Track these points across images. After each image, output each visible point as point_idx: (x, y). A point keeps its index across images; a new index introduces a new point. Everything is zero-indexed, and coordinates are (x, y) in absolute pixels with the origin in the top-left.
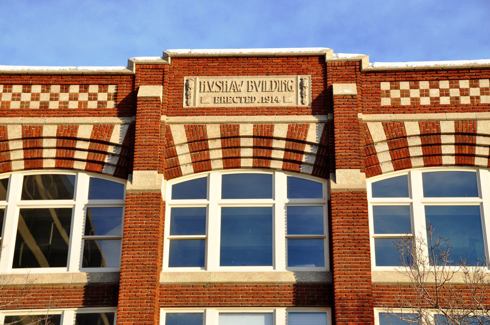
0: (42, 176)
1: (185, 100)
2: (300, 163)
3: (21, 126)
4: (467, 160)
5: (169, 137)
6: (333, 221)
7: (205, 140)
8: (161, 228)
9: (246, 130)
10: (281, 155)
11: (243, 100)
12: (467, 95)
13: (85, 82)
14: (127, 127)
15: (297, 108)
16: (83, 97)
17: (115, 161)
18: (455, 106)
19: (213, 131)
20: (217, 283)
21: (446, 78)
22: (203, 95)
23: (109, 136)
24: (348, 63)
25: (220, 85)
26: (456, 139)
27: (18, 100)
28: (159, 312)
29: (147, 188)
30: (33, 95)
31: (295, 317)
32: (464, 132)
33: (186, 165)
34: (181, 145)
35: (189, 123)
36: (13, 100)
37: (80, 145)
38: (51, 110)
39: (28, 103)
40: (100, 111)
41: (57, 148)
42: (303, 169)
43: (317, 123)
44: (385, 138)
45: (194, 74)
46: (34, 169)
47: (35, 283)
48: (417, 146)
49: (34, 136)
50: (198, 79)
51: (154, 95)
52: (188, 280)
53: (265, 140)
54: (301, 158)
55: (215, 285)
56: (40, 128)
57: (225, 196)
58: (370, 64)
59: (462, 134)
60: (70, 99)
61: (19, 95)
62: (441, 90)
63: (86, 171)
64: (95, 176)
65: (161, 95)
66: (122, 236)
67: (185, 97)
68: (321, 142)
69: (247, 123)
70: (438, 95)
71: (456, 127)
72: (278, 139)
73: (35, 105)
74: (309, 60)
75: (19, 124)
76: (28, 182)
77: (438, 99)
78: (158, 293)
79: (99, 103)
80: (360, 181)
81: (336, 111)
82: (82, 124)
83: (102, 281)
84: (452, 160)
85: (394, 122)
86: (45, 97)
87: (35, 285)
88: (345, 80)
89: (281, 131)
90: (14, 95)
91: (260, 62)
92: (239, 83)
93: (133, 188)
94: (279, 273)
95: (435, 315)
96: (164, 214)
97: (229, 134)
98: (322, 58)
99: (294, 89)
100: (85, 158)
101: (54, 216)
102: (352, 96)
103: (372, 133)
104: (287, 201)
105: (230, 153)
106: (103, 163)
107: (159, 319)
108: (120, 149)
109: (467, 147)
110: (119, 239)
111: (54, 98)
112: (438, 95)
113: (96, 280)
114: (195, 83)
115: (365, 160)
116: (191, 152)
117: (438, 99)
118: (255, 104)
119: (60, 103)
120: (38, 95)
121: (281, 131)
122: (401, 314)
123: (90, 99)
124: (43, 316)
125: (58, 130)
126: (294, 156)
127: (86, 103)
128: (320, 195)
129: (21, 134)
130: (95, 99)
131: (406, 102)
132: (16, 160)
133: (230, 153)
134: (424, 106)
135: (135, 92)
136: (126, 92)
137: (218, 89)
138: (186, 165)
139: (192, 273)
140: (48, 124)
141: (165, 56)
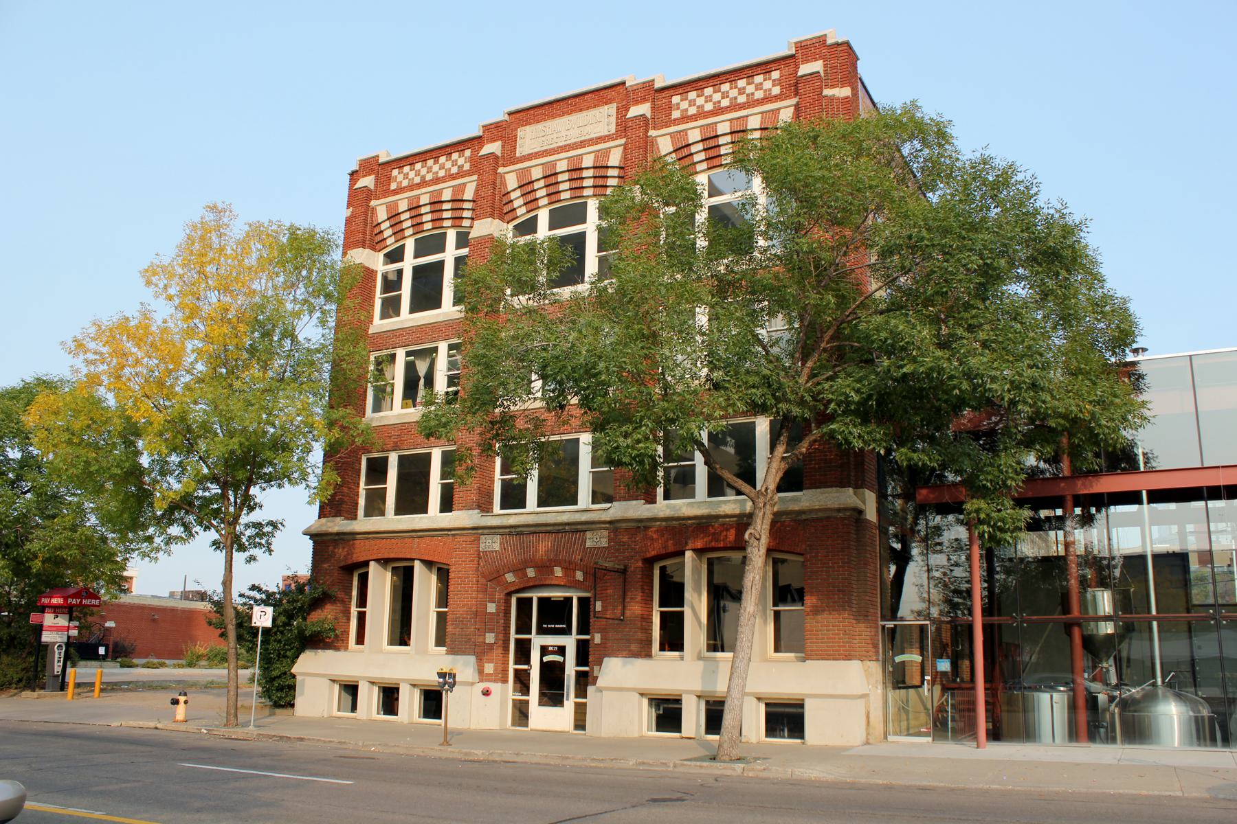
30: (690, 101)
63: (453, 226)
100: (449, 216)
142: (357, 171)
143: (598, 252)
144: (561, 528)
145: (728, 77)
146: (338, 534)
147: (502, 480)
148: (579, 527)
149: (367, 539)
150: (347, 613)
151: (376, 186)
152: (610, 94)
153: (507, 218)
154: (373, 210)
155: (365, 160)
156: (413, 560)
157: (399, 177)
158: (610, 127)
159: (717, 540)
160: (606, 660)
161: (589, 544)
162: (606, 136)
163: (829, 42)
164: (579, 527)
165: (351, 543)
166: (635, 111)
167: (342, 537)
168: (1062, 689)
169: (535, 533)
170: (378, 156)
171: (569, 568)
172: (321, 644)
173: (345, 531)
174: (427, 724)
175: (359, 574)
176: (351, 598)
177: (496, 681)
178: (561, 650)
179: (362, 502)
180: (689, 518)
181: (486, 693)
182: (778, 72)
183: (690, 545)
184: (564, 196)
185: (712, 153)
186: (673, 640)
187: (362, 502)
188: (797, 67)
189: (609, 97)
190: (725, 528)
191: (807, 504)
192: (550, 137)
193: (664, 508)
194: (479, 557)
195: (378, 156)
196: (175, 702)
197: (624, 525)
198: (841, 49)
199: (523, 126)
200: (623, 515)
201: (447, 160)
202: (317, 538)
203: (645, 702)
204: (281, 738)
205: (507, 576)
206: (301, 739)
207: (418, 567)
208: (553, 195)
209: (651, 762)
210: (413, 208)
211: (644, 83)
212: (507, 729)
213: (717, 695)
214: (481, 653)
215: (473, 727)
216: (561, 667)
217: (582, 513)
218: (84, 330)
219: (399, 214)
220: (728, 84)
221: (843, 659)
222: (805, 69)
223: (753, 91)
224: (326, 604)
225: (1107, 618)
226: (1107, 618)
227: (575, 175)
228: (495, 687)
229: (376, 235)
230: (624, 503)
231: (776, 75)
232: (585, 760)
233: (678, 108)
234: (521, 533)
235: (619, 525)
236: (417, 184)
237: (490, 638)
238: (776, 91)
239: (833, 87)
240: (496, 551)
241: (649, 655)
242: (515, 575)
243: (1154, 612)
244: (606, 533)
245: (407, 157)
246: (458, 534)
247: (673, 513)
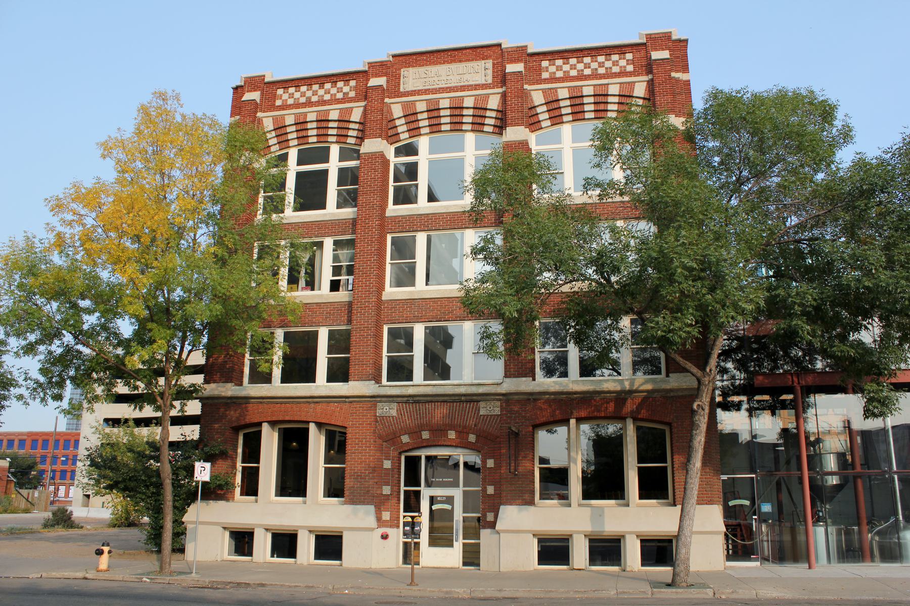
30: (302, 93)
36: (289, 98)
37: (289, 130)
39: (299, 99)
40: (346, 99)
62: (585, 64)
63: (337, 142)
70: (583, 68)
73: (303, 100)
79: (344, 94)
82: (332, 110)
86: (309, 94)
111: (315, 93)
112: (583, 68)
117: (582, 71)
119: (319, 97)
131: (560, 74)
142: (241, 87)
143: (338, 186)
144: (457, 398)
145: (589, 52)
146: (231, 398)
147: (388, 357)
148: (474, 398)
149: (261, 403)
150: (234, 467)
151: (261, 100)
152: (486, 52)
153: (391, 140)
154: (260, 121)
155: (250, 78)
156: (308, 422)
157: (549, 68)
158: (487, 78)
159: (599, 411)
160: (502, 507)
161: (482, 413)
162: (483, 85)
164: (474, 398)
165: (244, 405)
166: (511, 68)
167: (234, 400)
168: (821, 523)
169: (431, 402)
170: (264, 76)
171: (463, 432)
172: (213, 496)
173: (240, 395)
174: (334, 565)
175: (244, 434)
176: (237, 455)
177: (391, 526)
178: (450, 500)
179: (247, 370)
180: (576, 393)
181: (385, 537)
182: (355, 81)
183: (575, 414)
184: (311, 140)
185: (577, 109)
186: (251, 488)
187: (247, 370)
188: (368, 80)
189: (485, 54)
190: (608, 401)
191: (676, 385)
192: (431, 79)
193: (553, 384)
194: (376, 421)
195: (264, 76)
196: (100, 553)
197: (516, 397)
198: (682, 44)
199: (405, 67)
200: (516, 389)
201: (308, 90)
202: (206, 401)
203: (227, 534)
204: (239, 584)
205: (402, 437)
206: (263, 585)
207: (312, 428)
208: (302, 139)
209: (631, 591)
210: (300, 123)
211: (518, 47)
212: (399, 567)
213: (605, 534)
214: (380, 503)
215: (373, 566)
216: (449, 514)
217: (478, 386)
218: (67, 190)
219: (285, 126)
220: (590, 58)
221: (706, 504)
222: (374, 82)
223: (284, 95)
224: (218, 460)
225: (832, 474)
226: (832, 474)
227: (457, 112)
228: (391, 531)
229: (389, 129)
230: (515, 379)
231: (353, 83)
232: (568, 592)
233: (281, 99)
234: (418, 402)
235: (511, 397)
236: (303, 103)
237: (386, 490)
238: (630, 68)
239: (677, 71)
240: (393, 417)
241: (531, 503)
242: (410, 437)
243: (895, 468)
244: (498, 403)
245: (292, 80)
246: (355, 401)
247: (562, 388)
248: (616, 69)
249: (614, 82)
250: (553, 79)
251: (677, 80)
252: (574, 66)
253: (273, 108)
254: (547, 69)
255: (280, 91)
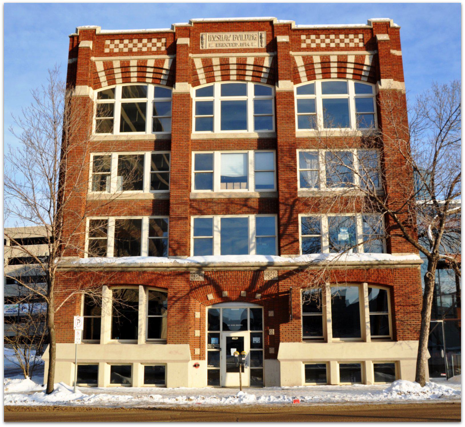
0: (131, 86)
1: (201, 45)
2: (260, 77)
3: (119, 61)
4: (343, 76)
5: (194, 65)
6: (277, 107)
7: (211, 66)
8: (190, 112)
9: (233, 60)
10: (251, 73)
11: (231, 45)
12: (343, 42)
13: (150, 37)
14: (172, 60)
15: (259, 49)
16: (149, 45)
17: (166, 78)
18: (338, 48)
19: (216, 62)
20: (219, 139)
21: (333, 33)
22: (210, 42)
23: (163, 65)
24: (285, 25)
25: (219, 37)
26: (338, 65)
27: (118, 47)
28: (191, 153)
29: (183, 91)
30: (125, 45)
31: (258, 155)
32: (342, 61)
33: (202, 79)
34: (200, 69)
35: (203, 57)
36: (115, 47)
37: (148, 70)
38: (134, 52)
39: (122, 49)
41: (138, 72)
42: (262, 80)
43: (269, 57)
44: (303, 64)
45: (206, 32)
46: (127, 82)
47: (131, 139)
48: (319, 68)
49: (126, 66)
50: (208, 34)
51: (185, 43)
52: (205, 137)
53: (243, 66)
54: (261, 75)
55: (218, 140)
56: (128, 62)
57: (222, 95)
58: (296, 26)
59: (341, 62)
60: (143, 46)
61: (118, 45)
62: (331, 40)
63: (152, 83)
64: (157, 86)
65: (189, 43)
66: (171, 116)
67: (201, 43)
68: (271, 66)
69: (233, 57)
71: (338, 59)
72: (249, 65)
74: (265, 23)
75: (118, 60)
76: (124, 88)
77: (329, 44)
78: (190, 144)
79: (158, 48)
80: (291, 86)
81: (279, 50)
82: (149, 59)
83: (162, 138)
84: (336, 76)
85: (308, 56)
87: (131, 140)
88: (283, 34)
89: (250, 61)
90: (115, 45)
91: (240, 24)
92: (228, 36)
93: (176, 92)
94: (250, 134)
95: (325, 152)
96: (192, 104)
97: (224, 63)
98: (271, 22)
99: (257, 39)
101: (138, 106)
102: (287, 42)
103: (297, 62)
104: (254, 97)
105: (225, 73)
106: (160, 79)
107: (191, 156)
108: (169, 72)
109: (343, 69)
110: (170, 117)
111: (135, 46)
113: (160, 138)
114: (206, 36)
115: (293, 76)
116: (205, 72)
118: (238, 47)
119: (138, 48)
120: (127, 44)
121: (250, 61)
122: (310, 152)
123: (153, 46)
124: (136, 155)
125: (138, 63)
126: (257, 74)
127: (151, 48)
128: (270, 94)
129: (120, 65)
130: (155, 46)
131: (313, 45)
132: (118, 78)
133: (225, 73)
134: (323, 48)
135: (175, 41)
136: (171, 41)
137: (218, 39)
138: (202, 79)
139: (207, 134)
140: (133, 59)
141: (190, 23)
163: (97, 32)
181: (196, 366)
231: (361, 36)
239: (394, 49)
248: (352, 45)
249: (352, 54)
250: (309, 48)
251: (394, 56)
252: (323, 41)
253: (101, 53)
254: (304, 41)
255: (108, 42)
